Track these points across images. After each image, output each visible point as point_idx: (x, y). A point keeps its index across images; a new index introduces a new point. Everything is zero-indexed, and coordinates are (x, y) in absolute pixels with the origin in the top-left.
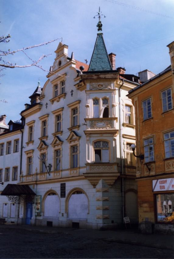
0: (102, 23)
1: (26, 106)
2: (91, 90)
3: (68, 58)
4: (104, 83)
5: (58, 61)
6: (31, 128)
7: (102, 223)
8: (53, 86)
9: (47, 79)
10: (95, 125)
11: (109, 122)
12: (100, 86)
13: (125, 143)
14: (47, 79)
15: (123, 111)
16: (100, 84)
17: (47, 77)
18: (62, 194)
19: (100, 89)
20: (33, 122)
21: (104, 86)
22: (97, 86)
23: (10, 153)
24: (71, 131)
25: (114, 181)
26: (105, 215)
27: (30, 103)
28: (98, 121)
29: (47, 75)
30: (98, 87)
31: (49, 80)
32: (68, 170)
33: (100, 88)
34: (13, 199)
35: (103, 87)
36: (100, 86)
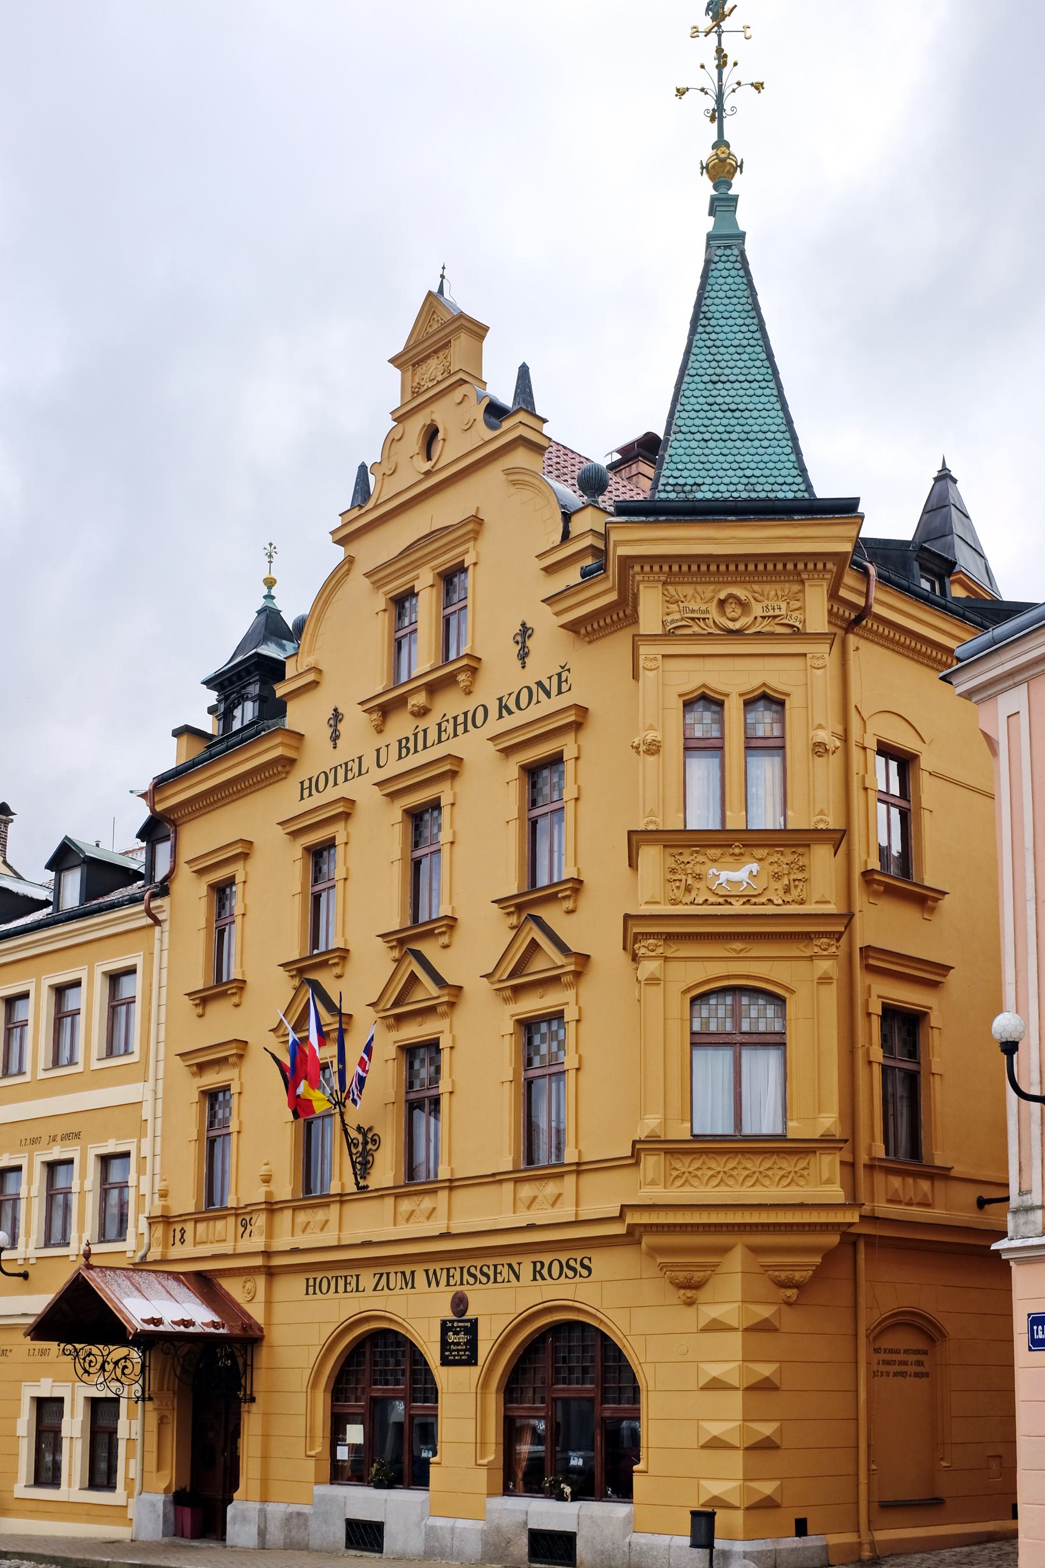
0: (737, 150)
1: (184, 738)
2: (669, 635)
3: (495, 412)
4: (756, 587)
5: (416, 426)
7: (259, 1477)
8: (381, 601)
9: (339, 553)
10: (698, 877)
11: (791, 858)
12: (732, 610)
13: (876, 1008)
14: (339, 553)
15: (866, 789)
16: (731, 596)
17: (339, 542)
18: (451, 1337)
19: (731, 625)
20: (339, 809)
21: (757, 610)
22: (713, 607)
23: (130, 1051)
24: (296, 982)
25: (817, 1260)
26: (755, 1485)
27: (208, 725)
28: (717, 852)
29: (338, 522)
30: (714, 614)
31: (350, 560)
32: (495, 1179)
33: (733, 620)
34: (103, 1368)
35: (750, 620)
36: (732, 610)
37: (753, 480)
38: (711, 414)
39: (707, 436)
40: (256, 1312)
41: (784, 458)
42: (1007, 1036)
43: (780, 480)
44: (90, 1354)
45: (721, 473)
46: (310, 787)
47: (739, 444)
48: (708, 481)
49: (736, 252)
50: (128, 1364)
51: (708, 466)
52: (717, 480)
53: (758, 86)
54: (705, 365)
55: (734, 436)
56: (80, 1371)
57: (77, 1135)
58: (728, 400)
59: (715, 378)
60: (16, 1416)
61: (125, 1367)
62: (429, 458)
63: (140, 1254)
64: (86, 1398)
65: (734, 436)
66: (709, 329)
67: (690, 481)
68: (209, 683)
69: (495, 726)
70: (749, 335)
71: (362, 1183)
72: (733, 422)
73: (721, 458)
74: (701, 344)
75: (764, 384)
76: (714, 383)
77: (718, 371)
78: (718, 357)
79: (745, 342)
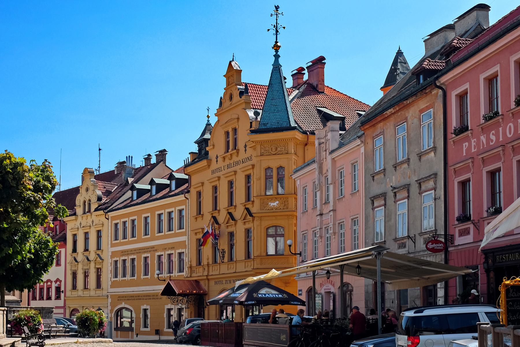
6: (199, 194)
37: (279, 121)
38: (271, 107)
39: (270, 112)
40: (206, 288)
41: (285, 116)
42: (290, 244)
43: (284, 121)
44: (174, 298)
45: (273, 120)
46: (213, 172)
47: (276, 113)
48: (270, 122)
49: (278, 68)
50: (183, 300)
51: (270, 119)
52: (272, 122)
53: (284, 28)
54: (271, 96)
55: (275, 111)
56: (172, 302)
57: (174, 248)
58: (275, 103)
59: (272, 99)
60: (140, 313)
61: (183, 301)
62: (231, 101)
63: (187, 275)
64: (167, 309)
65: (275, 111)
66: (272, 87)
67: (266, 122)
68: (195, 142)
69: (112, 277)
70: (280, 88)
71: (223, 261)
72: (275, 108)
73: (273, 117)
74: (270, 91)
75: (282, 99)
76: (272, 100)
77: (273, 97)
78: (273, 94)
79: (279, 90)
